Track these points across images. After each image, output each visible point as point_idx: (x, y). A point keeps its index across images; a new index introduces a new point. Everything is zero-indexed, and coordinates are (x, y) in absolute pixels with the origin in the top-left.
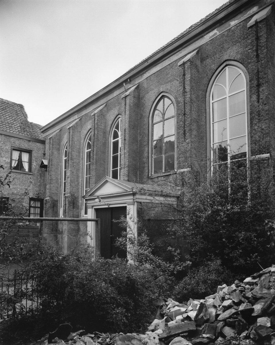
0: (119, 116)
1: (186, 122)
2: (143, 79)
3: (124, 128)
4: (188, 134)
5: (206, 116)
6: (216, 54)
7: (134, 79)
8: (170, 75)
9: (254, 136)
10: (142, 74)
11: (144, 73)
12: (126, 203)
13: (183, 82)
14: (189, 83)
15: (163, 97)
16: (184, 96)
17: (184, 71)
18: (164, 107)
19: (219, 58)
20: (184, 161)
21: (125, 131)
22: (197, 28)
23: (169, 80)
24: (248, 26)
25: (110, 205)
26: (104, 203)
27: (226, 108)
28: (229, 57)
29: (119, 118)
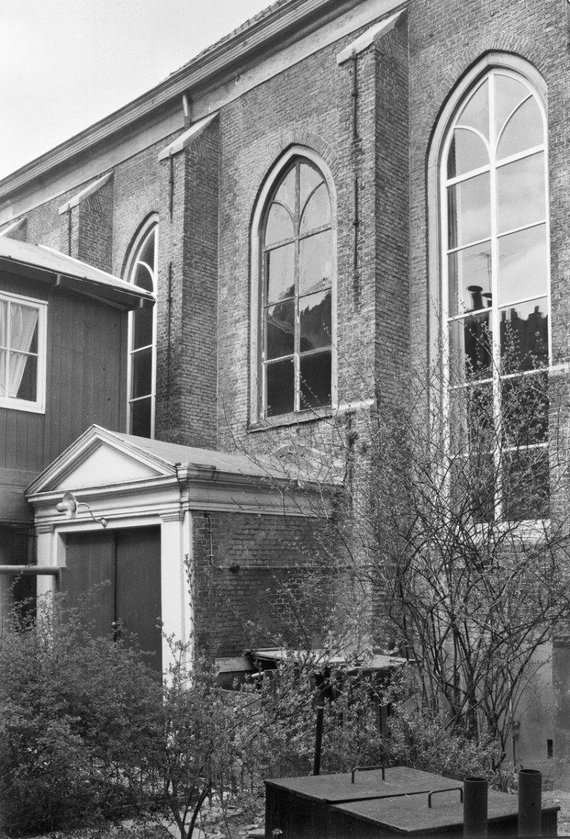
0: (155, 218)
1: (360, 249)
2: (231, 98)
3: (168, 260)
4: (366, 287)
5: (427, 230)
6: (457, 29)
7: (204, 95)
8: (317, 91)
9: (561, 302)
10: (230, 81)
11: (235, 78)
12: (157, 515)
13: (352, 117)
14: (371, 122)
15: (297, 163)
16: (357, 163)
17: (356, 82)
18: (298, 196)
19: (467, 44)
20: (355, 377)
21: (171, 272)
22: (271, 18)
23: (314, 105)
24: (160, 159)
25: (107, 520)
26: (89, 515)
27: (544, 183)
28: (497, 40)
29: (155, 223)
